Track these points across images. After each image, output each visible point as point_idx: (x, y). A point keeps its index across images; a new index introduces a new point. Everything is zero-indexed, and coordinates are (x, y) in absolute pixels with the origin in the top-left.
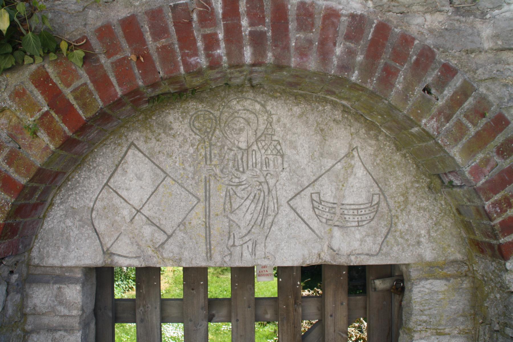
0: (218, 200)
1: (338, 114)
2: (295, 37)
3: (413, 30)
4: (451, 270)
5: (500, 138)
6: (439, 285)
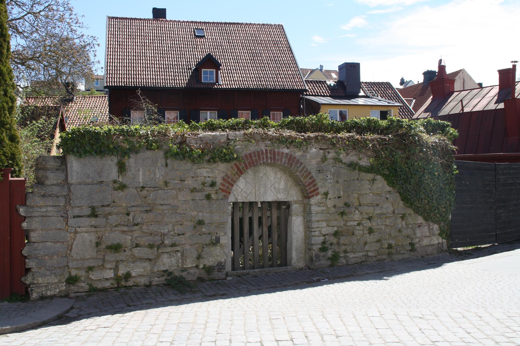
0: (257, 188)
1: (278, 169)
2: (277, 157)
3: (296, 156)
4: (299, 202)
5: (310, 176)
6: (297, 205)
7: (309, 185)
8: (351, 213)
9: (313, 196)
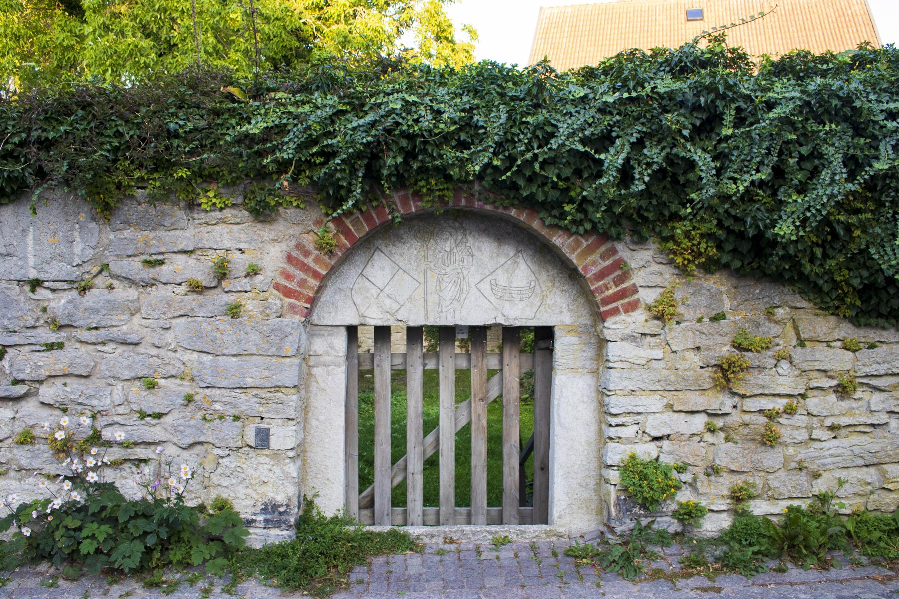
7: (601, 275)
8: (761, 369)
9: (615, 312)
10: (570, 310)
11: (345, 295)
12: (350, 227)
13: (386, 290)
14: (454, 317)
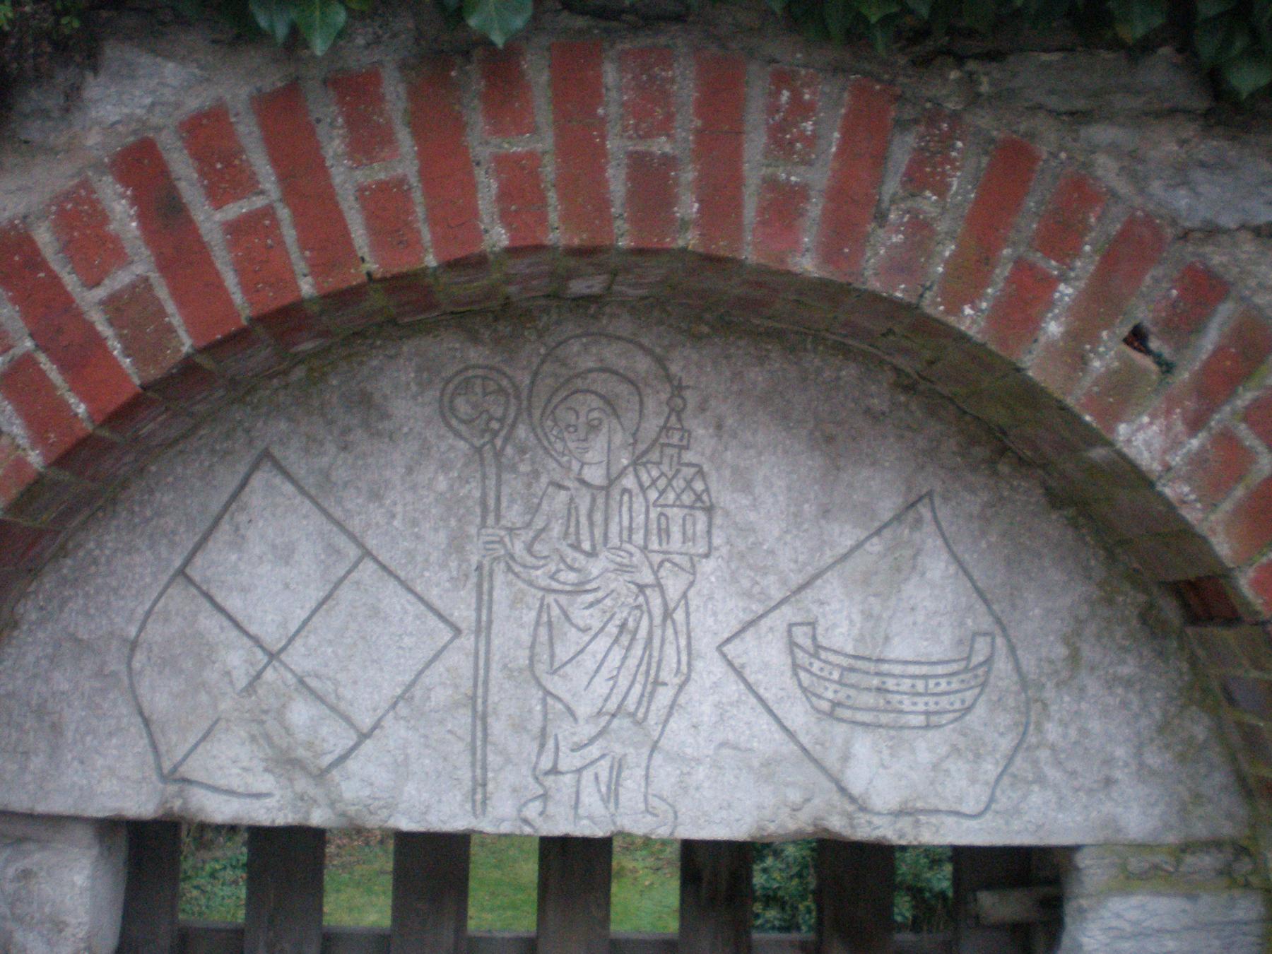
10: (1144, 773)
11: (100, 674)
12: (170, 307)
13: (298, 658)
14: (612, 794)
